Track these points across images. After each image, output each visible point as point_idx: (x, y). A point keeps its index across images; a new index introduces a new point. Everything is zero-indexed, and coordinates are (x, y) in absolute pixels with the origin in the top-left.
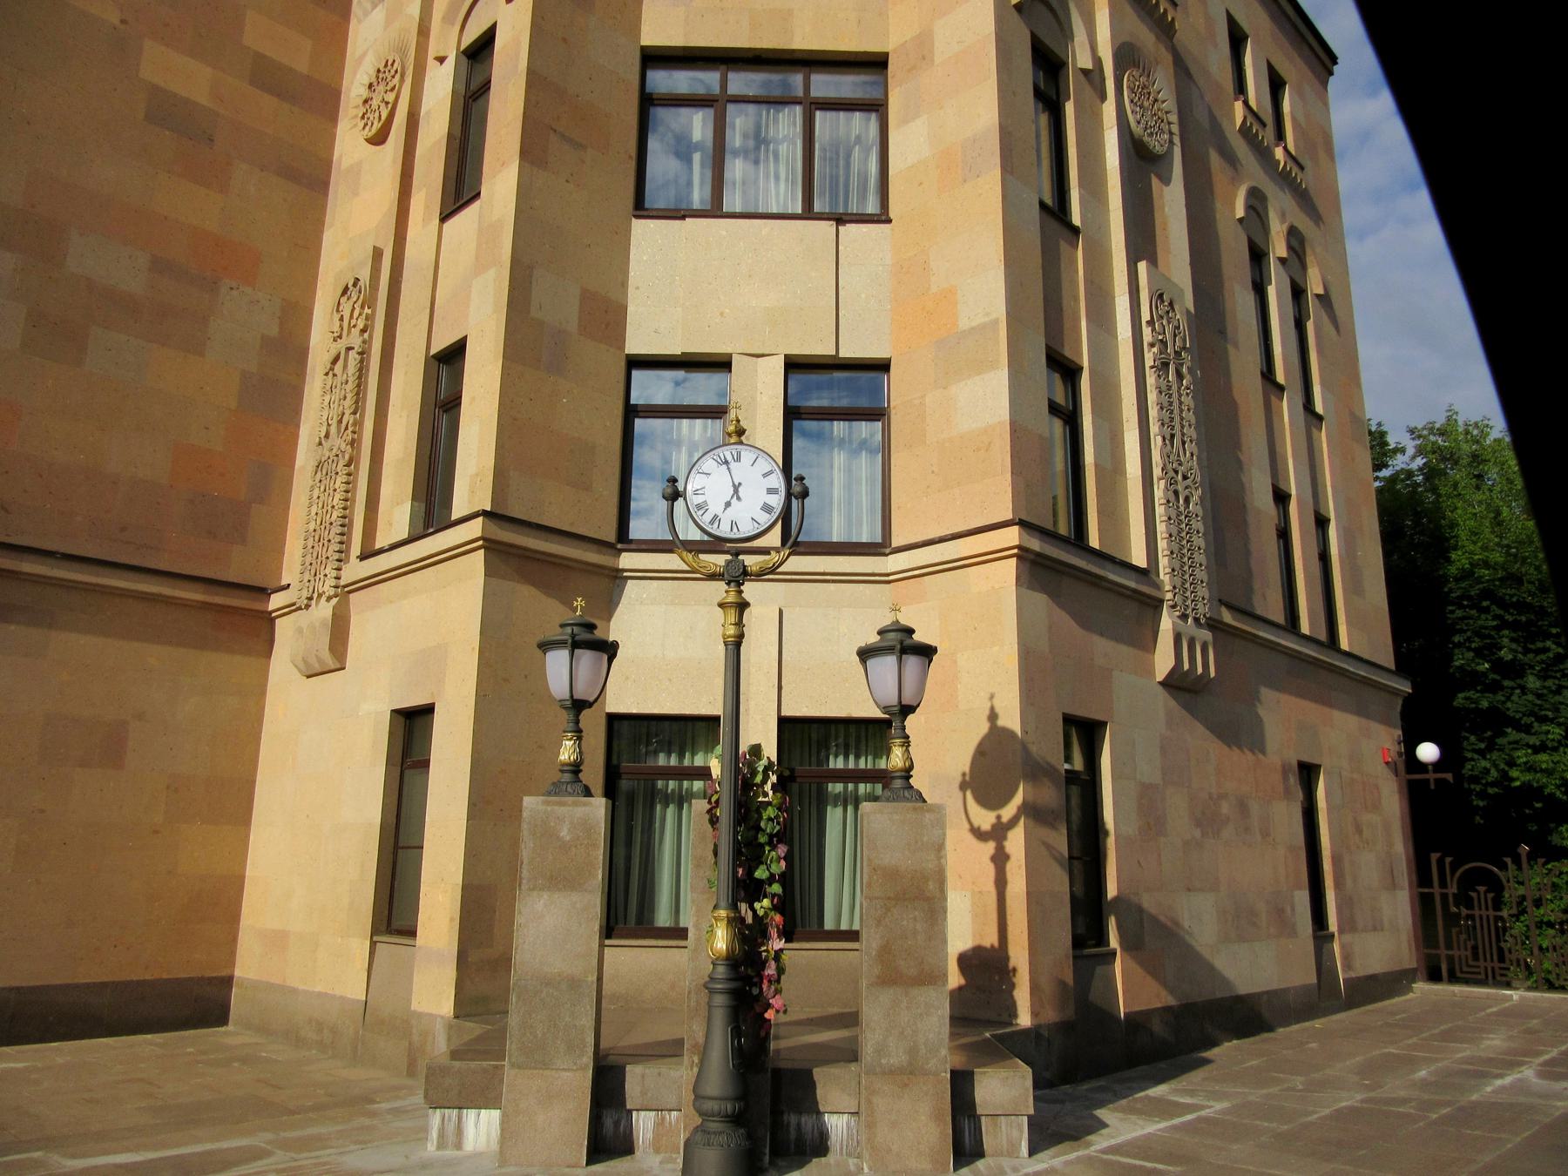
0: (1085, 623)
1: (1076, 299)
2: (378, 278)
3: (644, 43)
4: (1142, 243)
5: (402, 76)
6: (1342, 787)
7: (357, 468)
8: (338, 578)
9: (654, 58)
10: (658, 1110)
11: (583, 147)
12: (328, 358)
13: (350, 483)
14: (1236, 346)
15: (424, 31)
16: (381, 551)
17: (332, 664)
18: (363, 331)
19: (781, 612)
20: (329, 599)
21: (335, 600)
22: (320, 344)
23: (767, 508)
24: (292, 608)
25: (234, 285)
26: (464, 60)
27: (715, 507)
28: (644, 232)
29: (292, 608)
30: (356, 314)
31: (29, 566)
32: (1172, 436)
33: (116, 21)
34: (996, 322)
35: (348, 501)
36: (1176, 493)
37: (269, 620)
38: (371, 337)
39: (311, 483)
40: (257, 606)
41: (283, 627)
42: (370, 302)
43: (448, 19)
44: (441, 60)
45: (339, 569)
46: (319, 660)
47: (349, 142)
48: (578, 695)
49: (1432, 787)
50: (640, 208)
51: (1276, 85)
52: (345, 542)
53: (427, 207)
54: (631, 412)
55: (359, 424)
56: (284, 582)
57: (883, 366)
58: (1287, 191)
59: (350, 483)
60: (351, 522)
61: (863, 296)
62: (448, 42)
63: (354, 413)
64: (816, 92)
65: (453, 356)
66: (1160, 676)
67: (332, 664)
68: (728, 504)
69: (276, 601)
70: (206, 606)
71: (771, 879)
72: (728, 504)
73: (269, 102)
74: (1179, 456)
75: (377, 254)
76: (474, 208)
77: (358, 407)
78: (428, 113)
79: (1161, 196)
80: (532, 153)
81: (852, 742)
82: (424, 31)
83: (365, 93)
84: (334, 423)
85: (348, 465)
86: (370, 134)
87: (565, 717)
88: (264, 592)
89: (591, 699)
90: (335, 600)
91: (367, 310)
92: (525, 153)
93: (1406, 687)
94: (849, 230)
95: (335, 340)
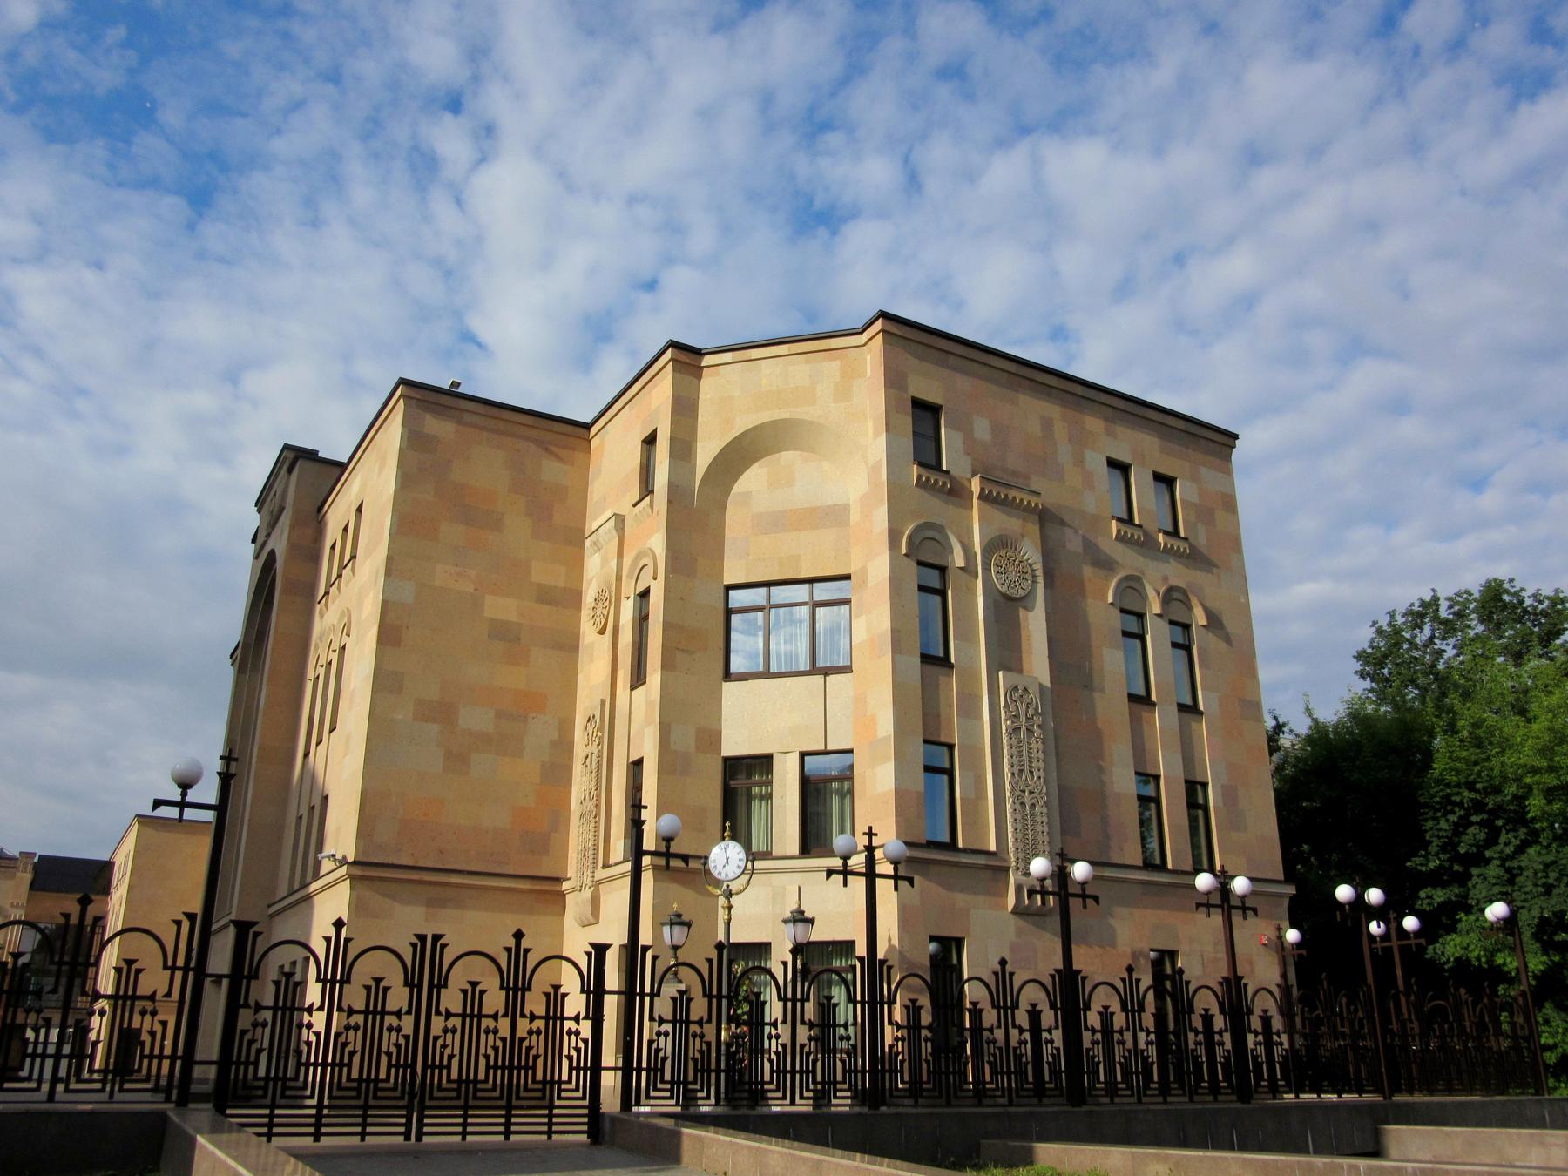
0: (949, 887)
1: (951, 706)
2: (604, 716)
3: (725, 583)
4: (1006, 651)
5: (610, 602)
6: (1203, 964)
7: (599, 819)
8: (593, 877)
9: (729, 588)
10: (729, 612)
11: (693, 652)
12: (584, 755)
13: (597, 826)
14: (1102, 690)
15: (619, 578)
16: (611, 866)
17: (592, 921)
18: (599, 745)
19: (799, 888)
20: (590, 888)
21: (592, 889)
22: (580, 751)
23: (739, 867)
24: (573, 890)
25: (534, 715)
26: (638, 598)
27: (720, 867)
28: (728, 687)
29: (573, 890)
30: (595, 735)
31: (455, 879)
32: (1021, 771)
33: (472, 591)
34: (890, 736)
35: (596, 836)
36: (1023, 804)
37: (562, 895)
38: (602, 748)
39: (578, 824)
40: (556, 888)
41: (570, 899)
42: (601, 729)
43: (629, 577)
44: (628, 598)
45: (593, 872)
46: (588, 920)
47: (588, 631)
48: (676, 942)
49: (1380, 953)
50: (728, 675)
51: (1165, 481)
52: (595, 863)
53: (624, 682)
54: (729, 612)
55: (599, 795)
56: (569, 876)
57: (851, 751)
58: (1171, 561)
59: (597, 826)
60: (598, 847)
61: (839, 714)
62: (630, 590)
63: (597, 789)
64: (817, 598)
65: (638, 763)
66: (1010, 910)
67: (592, 921)
68: (724, 866)
69: (566, 886)
70: (531, 891)
71: (744, 1014)
72: (724, 866)
73: (545, 608)
74: (1026, 780)
75: (603, 702)
76: (644, 687)
77: (598, 786)
78: (623, 625)
79: (1027, 620)
80: (666, 665)
81: (844, 953)
82: (619, 578)
83: (593, 605)
84: (587, 793)
85: (595, 817)
86: (598, 629)
87: (671, 952)
88: (558, 880)
89: (681, 944)
90: (592, 889)
91: (600, 734)
92: (663, 667)
93: (1291, 890)
94: (832, 679)
95: (586, 746)
